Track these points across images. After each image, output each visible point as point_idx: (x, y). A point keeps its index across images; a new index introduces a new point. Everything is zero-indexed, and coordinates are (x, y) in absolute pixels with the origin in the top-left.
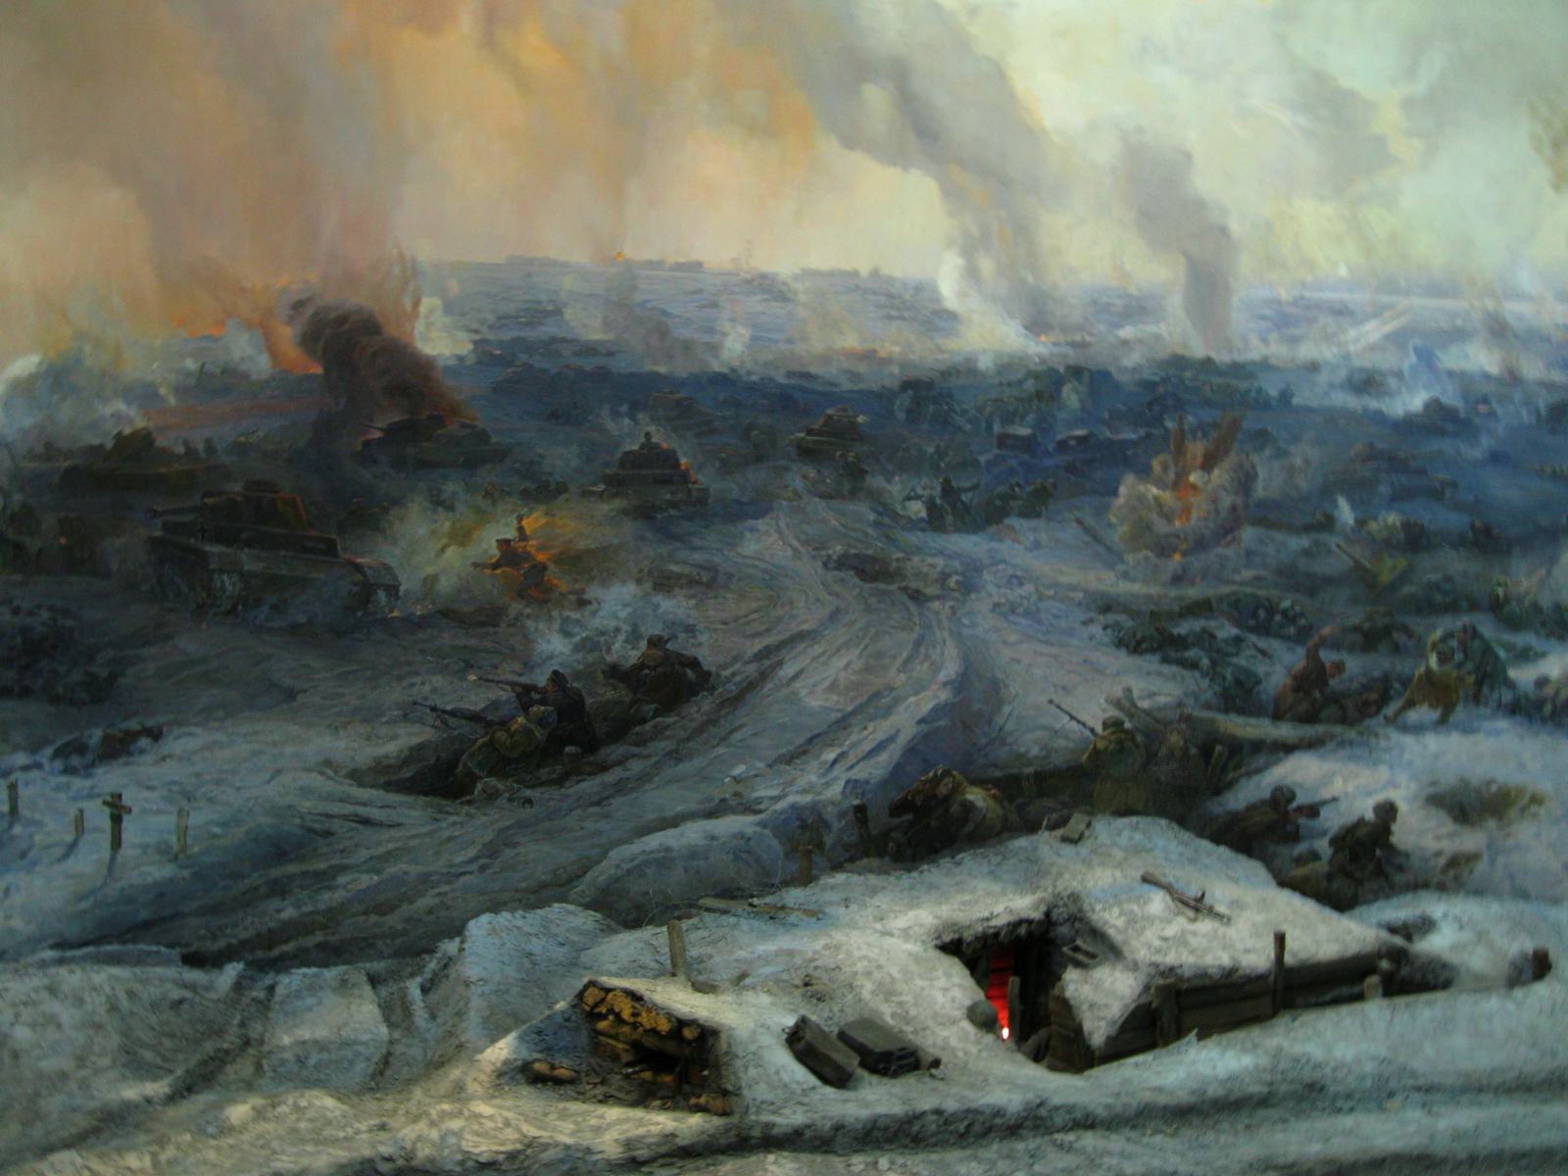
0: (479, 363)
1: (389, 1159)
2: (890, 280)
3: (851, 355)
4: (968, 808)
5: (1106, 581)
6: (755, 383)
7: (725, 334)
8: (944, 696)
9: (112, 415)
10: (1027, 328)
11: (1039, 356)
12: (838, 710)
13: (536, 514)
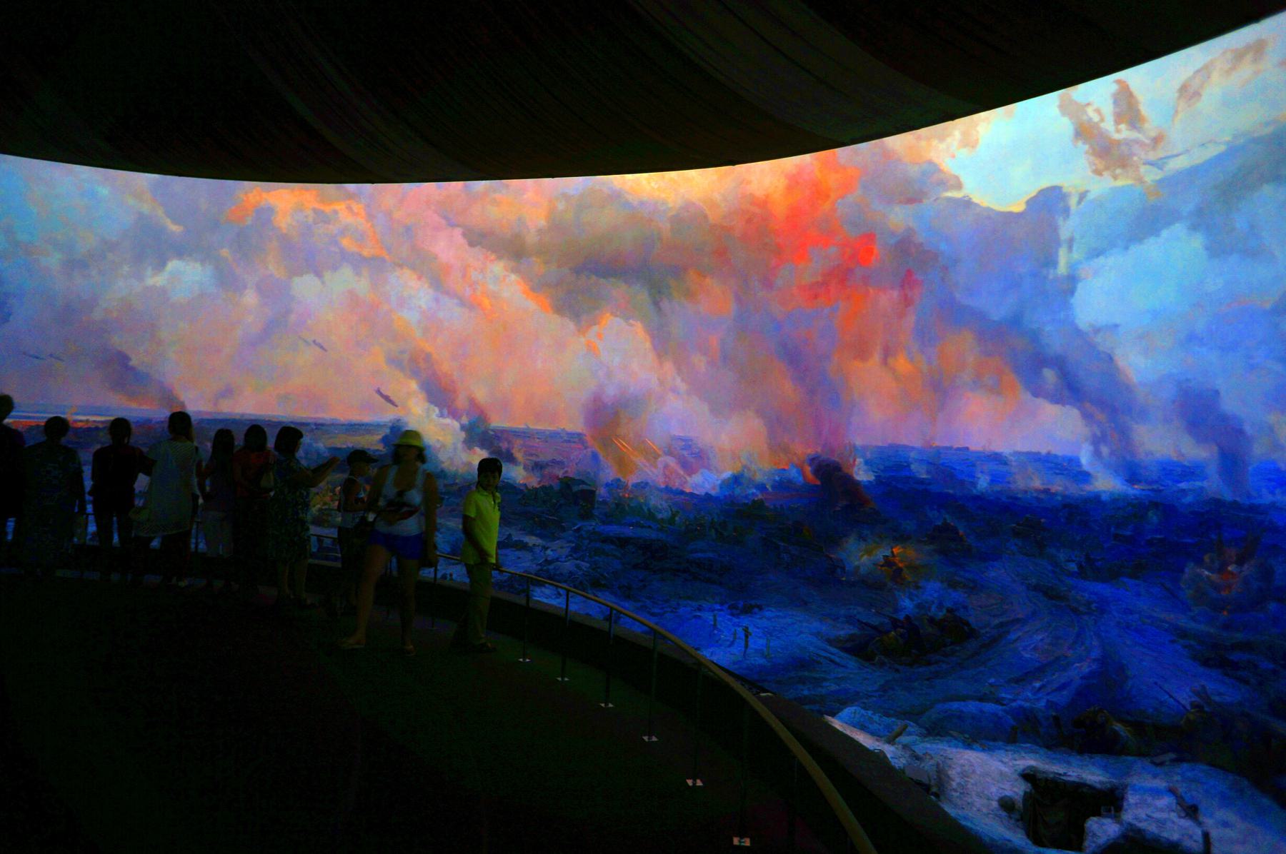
2: (1056, 456)
3: (1037, 490)
4: (1116, 733)
10: (1127, 481)
11: (1134, 495)
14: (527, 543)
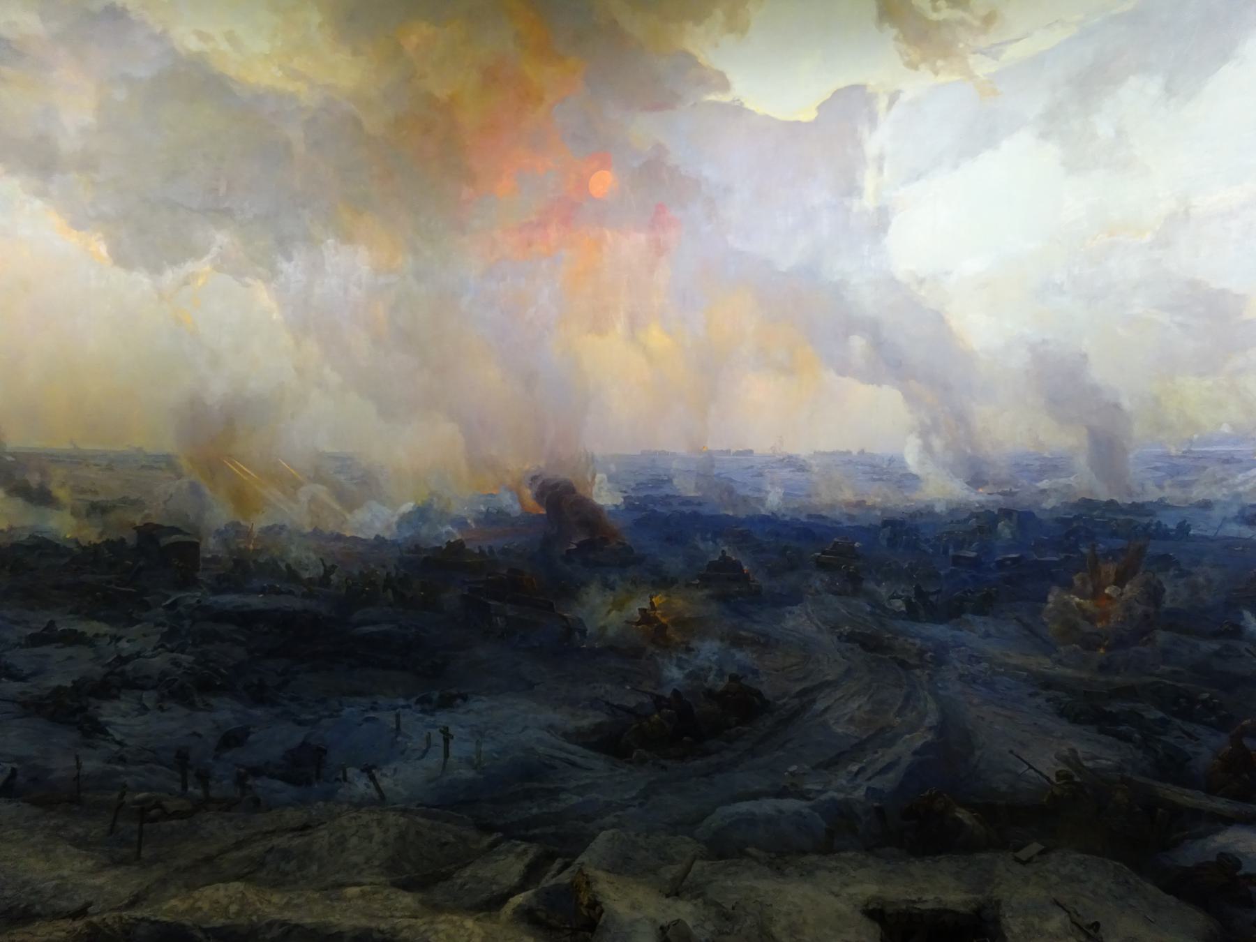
0: (627, 508)
1: (382, 932)
3: (848, 504)
5: (1043, 664)
6: (787, 522)
7: (768, 492)
8: (930, 737)
9: (446, 532)
10: (968, 483)
11: (978, 502)
12: (856, 737)
13: (660, 595)
14: (83, 633)
